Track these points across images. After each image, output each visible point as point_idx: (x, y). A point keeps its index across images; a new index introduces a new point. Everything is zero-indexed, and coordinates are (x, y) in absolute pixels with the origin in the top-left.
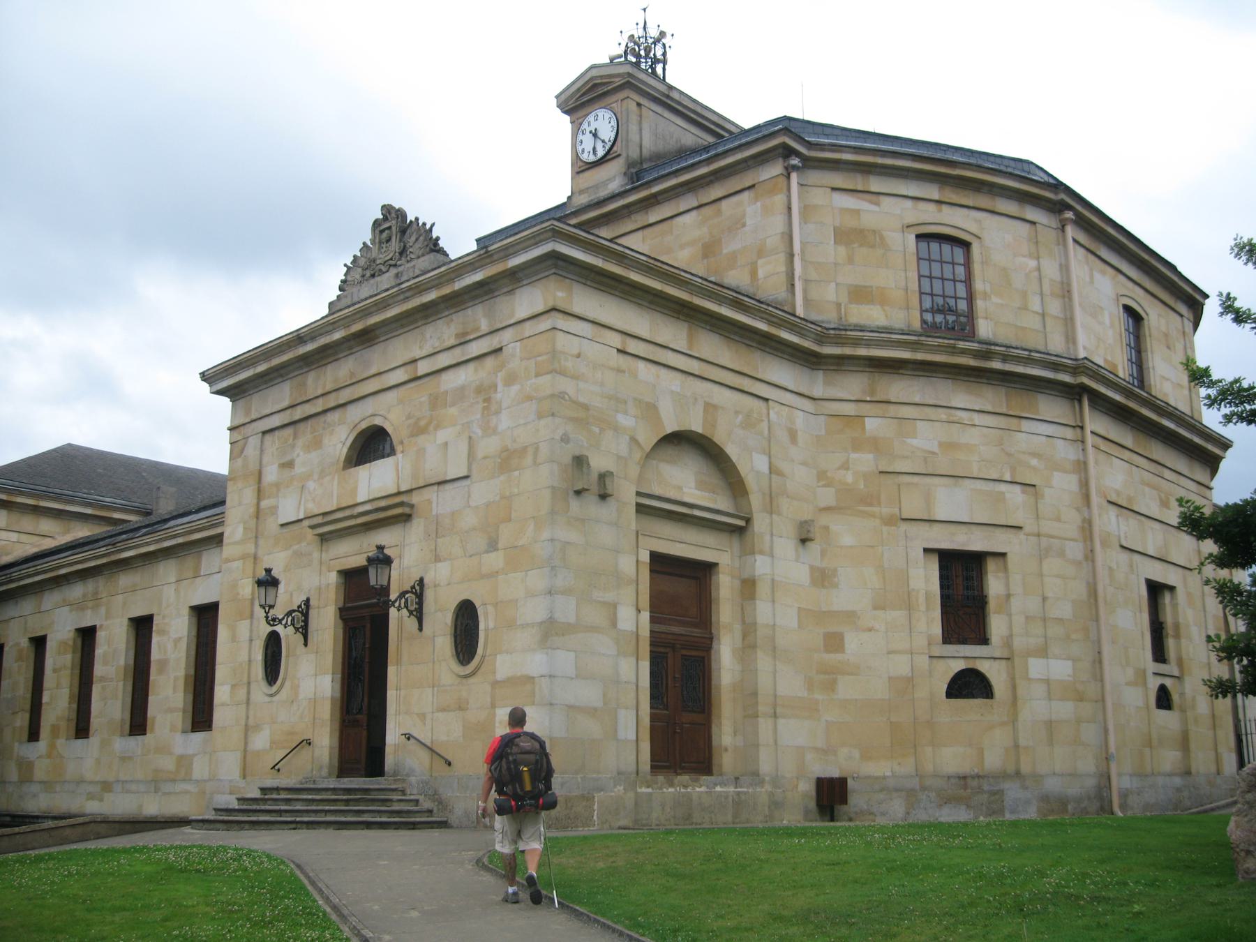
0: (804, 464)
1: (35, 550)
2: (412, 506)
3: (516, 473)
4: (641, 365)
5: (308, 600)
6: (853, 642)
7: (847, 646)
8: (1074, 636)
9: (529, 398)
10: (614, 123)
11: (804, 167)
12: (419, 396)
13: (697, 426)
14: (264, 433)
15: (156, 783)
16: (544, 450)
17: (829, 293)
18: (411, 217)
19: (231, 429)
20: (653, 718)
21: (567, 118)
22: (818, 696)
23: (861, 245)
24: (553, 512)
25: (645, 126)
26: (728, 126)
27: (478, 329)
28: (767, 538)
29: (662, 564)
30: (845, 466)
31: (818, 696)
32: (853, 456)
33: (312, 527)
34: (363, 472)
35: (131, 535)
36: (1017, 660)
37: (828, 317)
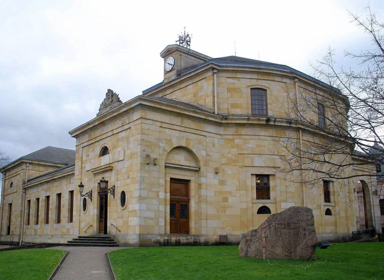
0: (218, 152)
2: (113, 167)
3: (133, 159)
4: (167, 130)
5: (92, 190)
6: (231, 199)
7: (229, 200)
8: (295, 196)
9: (136, 140)
10: (173, 60)
11: (218, 72)
12: (114, 138)
14: (83, 147)
16: (139, 154)
17: (225, 106)
18: (114, 93)
20: (171, 220)
21: (163, 59)
24: (141, 169)
25: (182, 61)
26: (208, 58)
27: (126, 122)
28: (205, 172)
29: (173, 180)
30: (229, 153)
32: (231, 150)
33: (92, 172)
34: (103, 158)
35: (56, 172)
36: (277, 204)
37: (224, 112)
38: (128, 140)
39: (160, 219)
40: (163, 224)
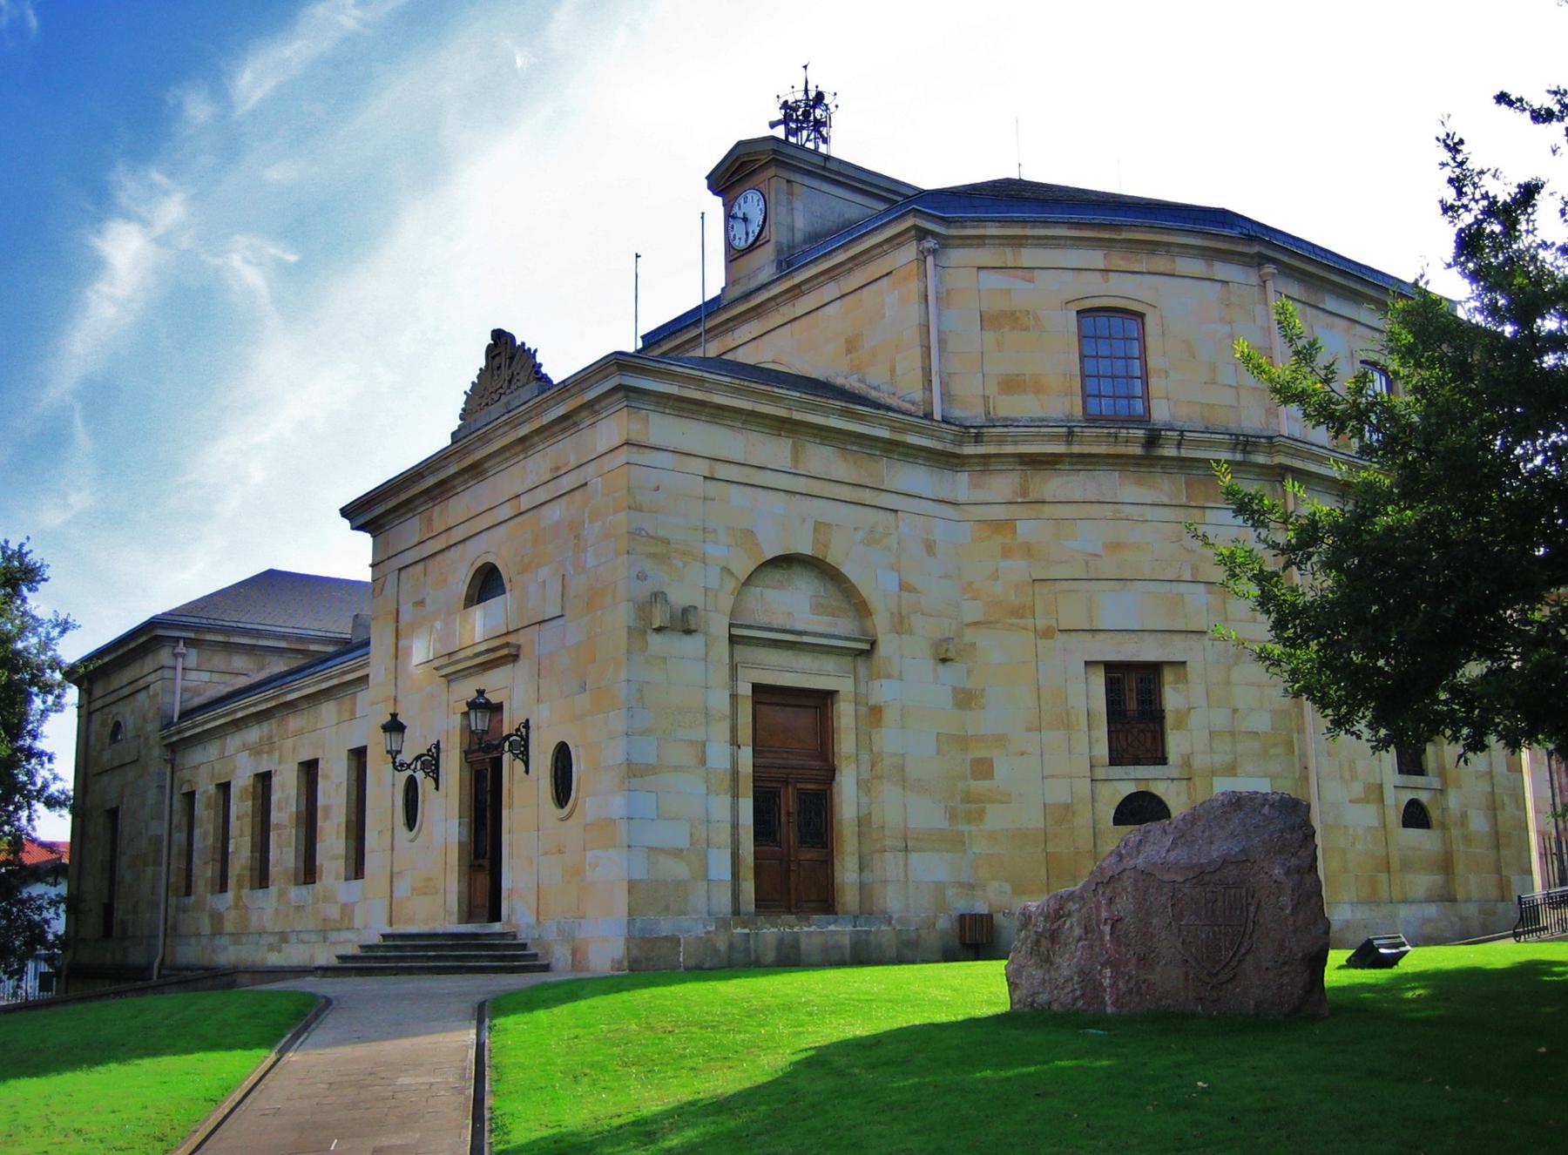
1: (230, 689)
13: (806, 549)
15: (325, 931)
19: (372, 566)
21: (719, 200)
22: (965, 828)
23: (1013, 328)
30: (995, 576)
31: (965, 828)
34: (478, 612)
37: (971, 412)
38: (577, 537)
39: (713, 854)
40: (727, 875)
